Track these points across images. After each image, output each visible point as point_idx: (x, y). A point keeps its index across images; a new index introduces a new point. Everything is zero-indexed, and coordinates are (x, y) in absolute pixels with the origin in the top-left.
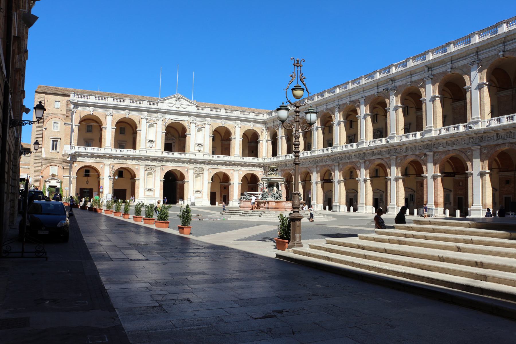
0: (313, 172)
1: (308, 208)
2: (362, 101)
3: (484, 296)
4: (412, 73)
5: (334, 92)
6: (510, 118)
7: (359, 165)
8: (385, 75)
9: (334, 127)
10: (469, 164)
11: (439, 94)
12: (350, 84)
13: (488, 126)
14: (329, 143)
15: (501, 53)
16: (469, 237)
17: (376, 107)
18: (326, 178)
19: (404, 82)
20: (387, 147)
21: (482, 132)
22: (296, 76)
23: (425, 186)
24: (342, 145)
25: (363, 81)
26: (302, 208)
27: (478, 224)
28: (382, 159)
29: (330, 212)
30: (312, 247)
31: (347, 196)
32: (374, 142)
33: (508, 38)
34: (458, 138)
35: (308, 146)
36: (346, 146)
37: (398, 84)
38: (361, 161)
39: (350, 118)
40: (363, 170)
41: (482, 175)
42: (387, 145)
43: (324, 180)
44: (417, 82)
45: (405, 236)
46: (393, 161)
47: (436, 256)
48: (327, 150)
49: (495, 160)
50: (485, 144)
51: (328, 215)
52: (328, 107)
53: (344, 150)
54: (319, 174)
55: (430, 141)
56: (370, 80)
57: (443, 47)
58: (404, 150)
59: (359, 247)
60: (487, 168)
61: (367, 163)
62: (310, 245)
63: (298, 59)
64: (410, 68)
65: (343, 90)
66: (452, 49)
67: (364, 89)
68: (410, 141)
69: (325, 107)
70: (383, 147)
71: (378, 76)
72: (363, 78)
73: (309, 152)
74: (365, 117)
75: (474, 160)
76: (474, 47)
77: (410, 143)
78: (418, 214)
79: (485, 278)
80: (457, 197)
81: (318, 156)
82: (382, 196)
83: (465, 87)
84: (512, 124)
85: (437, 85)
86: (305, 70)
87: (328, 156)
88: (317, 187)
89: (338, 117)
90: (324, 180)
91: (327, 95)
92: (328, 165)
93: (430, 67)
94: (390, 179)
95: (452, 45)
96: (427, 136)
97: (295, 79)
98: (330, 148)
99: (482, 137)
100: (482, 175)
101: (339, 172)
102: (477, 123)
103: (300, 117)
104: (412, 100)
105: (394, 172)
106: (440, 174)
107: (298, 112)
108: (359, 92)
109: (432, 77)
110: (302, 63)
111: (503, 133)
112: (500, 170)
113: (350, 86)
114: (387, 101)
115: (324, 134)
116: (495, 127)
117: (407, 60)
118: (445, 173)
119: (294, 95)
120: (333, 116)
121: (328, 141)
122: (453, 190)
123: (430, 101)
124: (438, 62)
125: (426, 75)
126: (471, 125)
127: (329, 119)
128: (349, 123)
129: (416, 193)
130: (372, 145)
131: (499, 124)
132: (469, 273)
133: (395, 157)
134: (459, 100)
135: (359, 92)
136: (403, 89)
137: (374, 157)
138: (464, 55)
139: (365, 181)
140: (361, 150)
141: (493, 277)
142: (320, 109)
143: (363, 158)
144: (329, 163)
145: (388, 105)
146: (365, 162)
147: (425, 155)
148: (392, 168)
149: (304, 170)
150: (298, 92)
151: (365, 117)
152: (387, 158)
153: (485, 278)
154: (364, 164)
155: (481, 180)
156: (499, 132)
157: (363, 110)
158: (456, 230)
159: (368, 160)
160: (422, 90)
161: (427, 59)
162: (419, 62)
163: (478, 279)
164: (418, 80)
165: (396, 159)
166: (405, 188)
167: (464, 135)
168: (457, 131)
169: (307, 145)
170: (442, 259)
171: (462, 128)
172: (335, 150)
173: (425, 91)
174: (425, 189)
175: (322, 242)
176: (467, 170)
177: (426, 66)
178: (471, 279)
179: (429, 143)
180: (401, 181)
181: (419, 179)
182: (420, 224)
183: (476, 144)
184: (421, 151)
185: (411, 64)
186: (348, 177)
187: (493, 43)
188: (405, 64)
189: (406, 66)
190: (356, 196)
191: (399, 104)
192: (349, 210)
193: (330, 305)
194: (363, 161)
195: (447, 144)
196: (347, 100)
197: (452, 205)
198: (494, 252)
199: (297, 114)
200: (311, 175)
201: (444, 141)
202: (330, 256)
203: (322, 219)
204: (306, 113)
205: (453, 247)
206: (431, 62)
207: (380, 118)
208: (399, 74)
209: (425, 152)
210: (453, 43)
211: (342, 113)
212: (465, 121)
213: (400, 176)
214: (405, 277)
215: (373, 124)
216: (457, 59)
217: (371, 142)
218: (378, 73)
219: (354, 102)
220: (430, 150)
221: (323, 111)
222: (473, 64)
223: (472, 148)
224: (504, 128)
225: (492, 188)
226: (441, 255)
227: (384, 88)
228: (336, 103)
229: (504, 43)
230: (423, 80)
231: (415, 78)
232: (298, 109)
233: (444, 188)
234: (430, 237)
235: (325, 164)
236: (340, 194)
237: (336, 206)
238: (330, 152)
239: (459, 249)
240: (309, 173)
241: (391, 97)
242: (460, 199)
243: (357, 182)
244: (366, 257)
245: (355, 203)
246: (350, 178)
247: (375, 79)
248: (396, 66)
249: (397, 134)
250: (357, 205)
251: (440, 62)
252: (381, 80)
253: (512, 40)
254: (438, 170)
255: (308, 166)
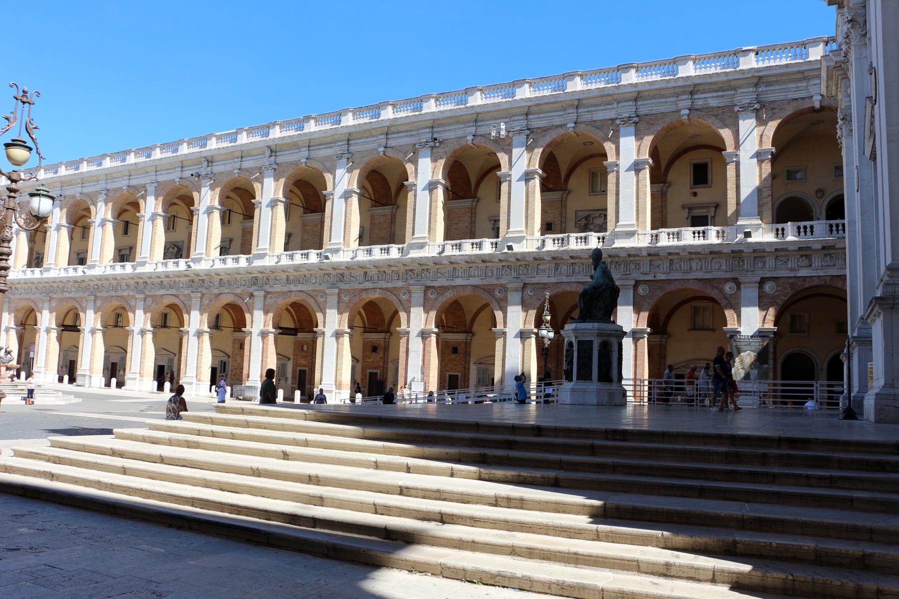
0: (43, 308)
1: (26, 379)
2: (151, 189)
3: (318, 530)
4: (243, 154)
5: (100, 164)
6: (476, 244)
7: (133, 304)
8: (197, 149)
9: (92, 229)
10: (319, 316)
11: (284, 196)
12: (132, 154)
13: (352, 258)
14: (79, 258)
15: (382, 149)
16: (302, 436)
17: (175, 204)
18: (69, 322)
19: (229, 168)
20: (186, 276)
21: (531, 259)
22: (18, 121)
23: (246, 347)
24: (104, 265)
25: (157, 154)
26: (702, 401)
27: (320, 414)
28: (176, 296)
29: (72, 387)
30: (18, 454)
31: (106, 358)
32: (166, 265)
33: (393, 129)
34: (306, 273)
35: (37, 258)
36: (112, 267)
37: (217, 168)
38: (137, 296)
39: (125, 217)
40: (140, 313)
41: (338, 335)
42: (187, 273)
43: (63, 326)
44: (250, 171)
45: (199, 433)
46: (196, 302)
47: (247, 468)
48: (75, 269)
49: (359, 313)
50: (346, 287)
51: (65, 393)
52: (85, 190)
53: (106, 273)
54: (54, 314)
55: (262, 273)
56: (169, 154)
57: (298, 121)
58: (217, 284)
59: (114, 453)
60: (346, 325)
61: (149, 300)
62: (14, 451)
63: (26, 89)
64: (241, 145)
65: (118, 163)
66: (312, 127)
67: (157, 168)
68: (228, 269)
69: (79, 190)
70: (179, 275)
71: (184, 150)
72: (158, 149)
73: (37, 270)
74: (153, 219)
75: (328, 311)
76: (345, 131)
77: (228, 272)
78: (232, 396)
79: (320, 501)
80: (448, 374)
81: (54, 280)
82: (171, 361)
83: (324, 192)
84: (704, 245)
85: (282, 181)
86: (38, 113)
87: (76, 282)
88: (48, 339)
89: (102, 212)
90: (63, 326)
91: (85, 168)
92: (74, 299)
93: (273, 150)
94: (188, 332)
95: (312, 122)
96: (257, 263)
97: (15, 125)
98: (80, 268)
99: (342, 275)
100: (338, 335)
101: (95, 313)
102: (337, 251)
103: (17, 200)
104: (238, 199)
105: (196, 321)
106: (274, 330)
107: (15, 191)
108: (147, 172)
109: (275, 167)
110: (34, 99)
111: (373, 272)
112: (366, 330)
113: (132, 159)
114: (195, 195)
115: (71, 238)
116: (363, 261)
117: (239, 131)
118: (281, 328)
119: (9, 157)
120: (92, 208)
121: (120, 251)
122: (292, 357)
123: (267, 206)
124: (288, 144)
125: (266, 161)
126: (329, 254)
127: (85, 213)
128: (122, 225)
129: (230, 359)
130: (161, 269)
131: (291, 263)
132: (297, 494)
133: (199, 295)
134: (313, 211)
135: (147, 172)
136: (226, 180)
137: (162, 292)
138: (329, 140)
139: (143, 333)
140: (140, 276)
141: (332, 499)
142: (69, 191)
143: (142, 292)
144: (77, 295)
145: (196, 202)
146: (145, 299)
147: (251, 295)
148: (510, 309)
149: (24, 304)
150: (19, 153)
151: (153, 219)
152: (185, 295)
153: (320, 501)
154: (142, 303)
155: (336, 344)
156: (367, 270)
157: (151, 205)
158: (283, 425)
159: (152, 296)
160: (257, 186)
161: (271, 136)
162: (257, 139)
163: (310, 504)
164: (252, 169)
165: (201, 298)
166: (213, 349)
167: (316, 269)
168: (306, 262)
169: (34, 256)
170: (257, 473)
171: (313, 257)
172: (90, 272)
173: (262, 188)
174: (246, 353)
175: (42, 445)
176: (317, 326)
177: (269, 147)
178: (300, 504)
179: (259, 275)
180: (206, 338)
181: (238, 335)
182: (226, 412)
183: (333, 285)
184: (245, 287)
185: (244, 139)
186: (112, 322)
187: (373, 131)
188: (233, 137)
189: (235, 140)
190: (124, 359)
191: (216, 203)
192: (108, 384)
193: (43, 567)
194: (142, 296)
195: (287, 280)
196: (123, 184)
197: (290, 381)
198: (339, 458)
199: (12, 194)
200: (38, 315)
201: (284, 276)
202: (53, 471)
203: (53, 399)
204: (32, 195)
205: (276, 451)
206: (277, 142)
207: (181, 224)
208: (222, 152)
209: (251, 290)
210: (581, 75)
211: (110, 205)
212: (602, 228)
213: (206, 328)
214: (193, 506)
215: (166, 232)
216: (319, 145)
217: (160, 265)
218: (185, 145)
219: (136, 188)
220: (261, 288)
221: (74, 196)
222: (341, 158)
223: (327, 291)
224: (376, 265)
225: (352, 357)
226: (255, 466)
227: (194, 172)
228: (102, 185)
229: (387, 134)
230: (260, 170)
231: (248, 164)
232: (14, 186)
233: (278, 354)
234: (241, 435)
235: (68, 295)
236: (92, 354)
237: (84, 376)
238: (80, 273)
239: (286, 456)
240: (33, 310)
241: (204, 190)
242: (302, 374)
243: (127, 334)
244: (124, 471)
245: (121, 372)
246: (116, 323)
247: (179, 154)
248: (219, 138)
249: (207, 254)
250: (124, 375)
251: (292, 145)
252: (190, 157)
253: (398, 132)
254: (271, 323)
255: (32, 297)
